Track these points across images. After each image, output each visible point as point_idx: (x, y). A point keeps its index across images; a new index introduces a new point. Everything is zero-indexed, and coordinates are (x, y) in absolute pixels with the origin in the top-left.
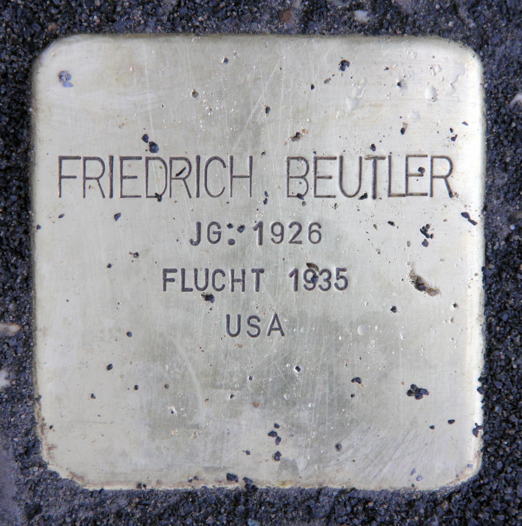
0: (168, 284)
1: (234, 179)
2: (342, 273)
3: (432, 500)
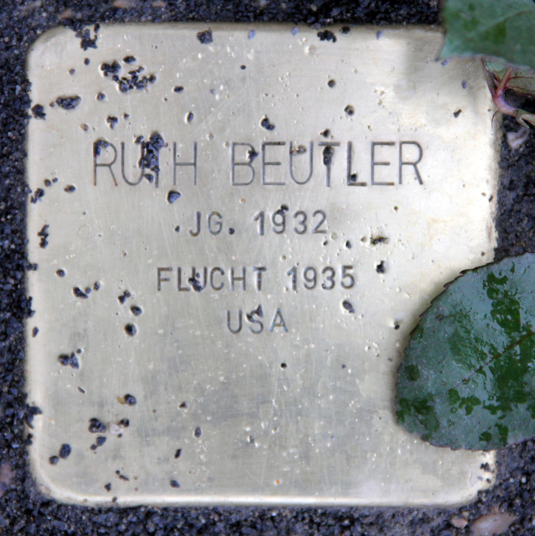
0: (162, 283)
1: (376, 167)
2: (350, 272)
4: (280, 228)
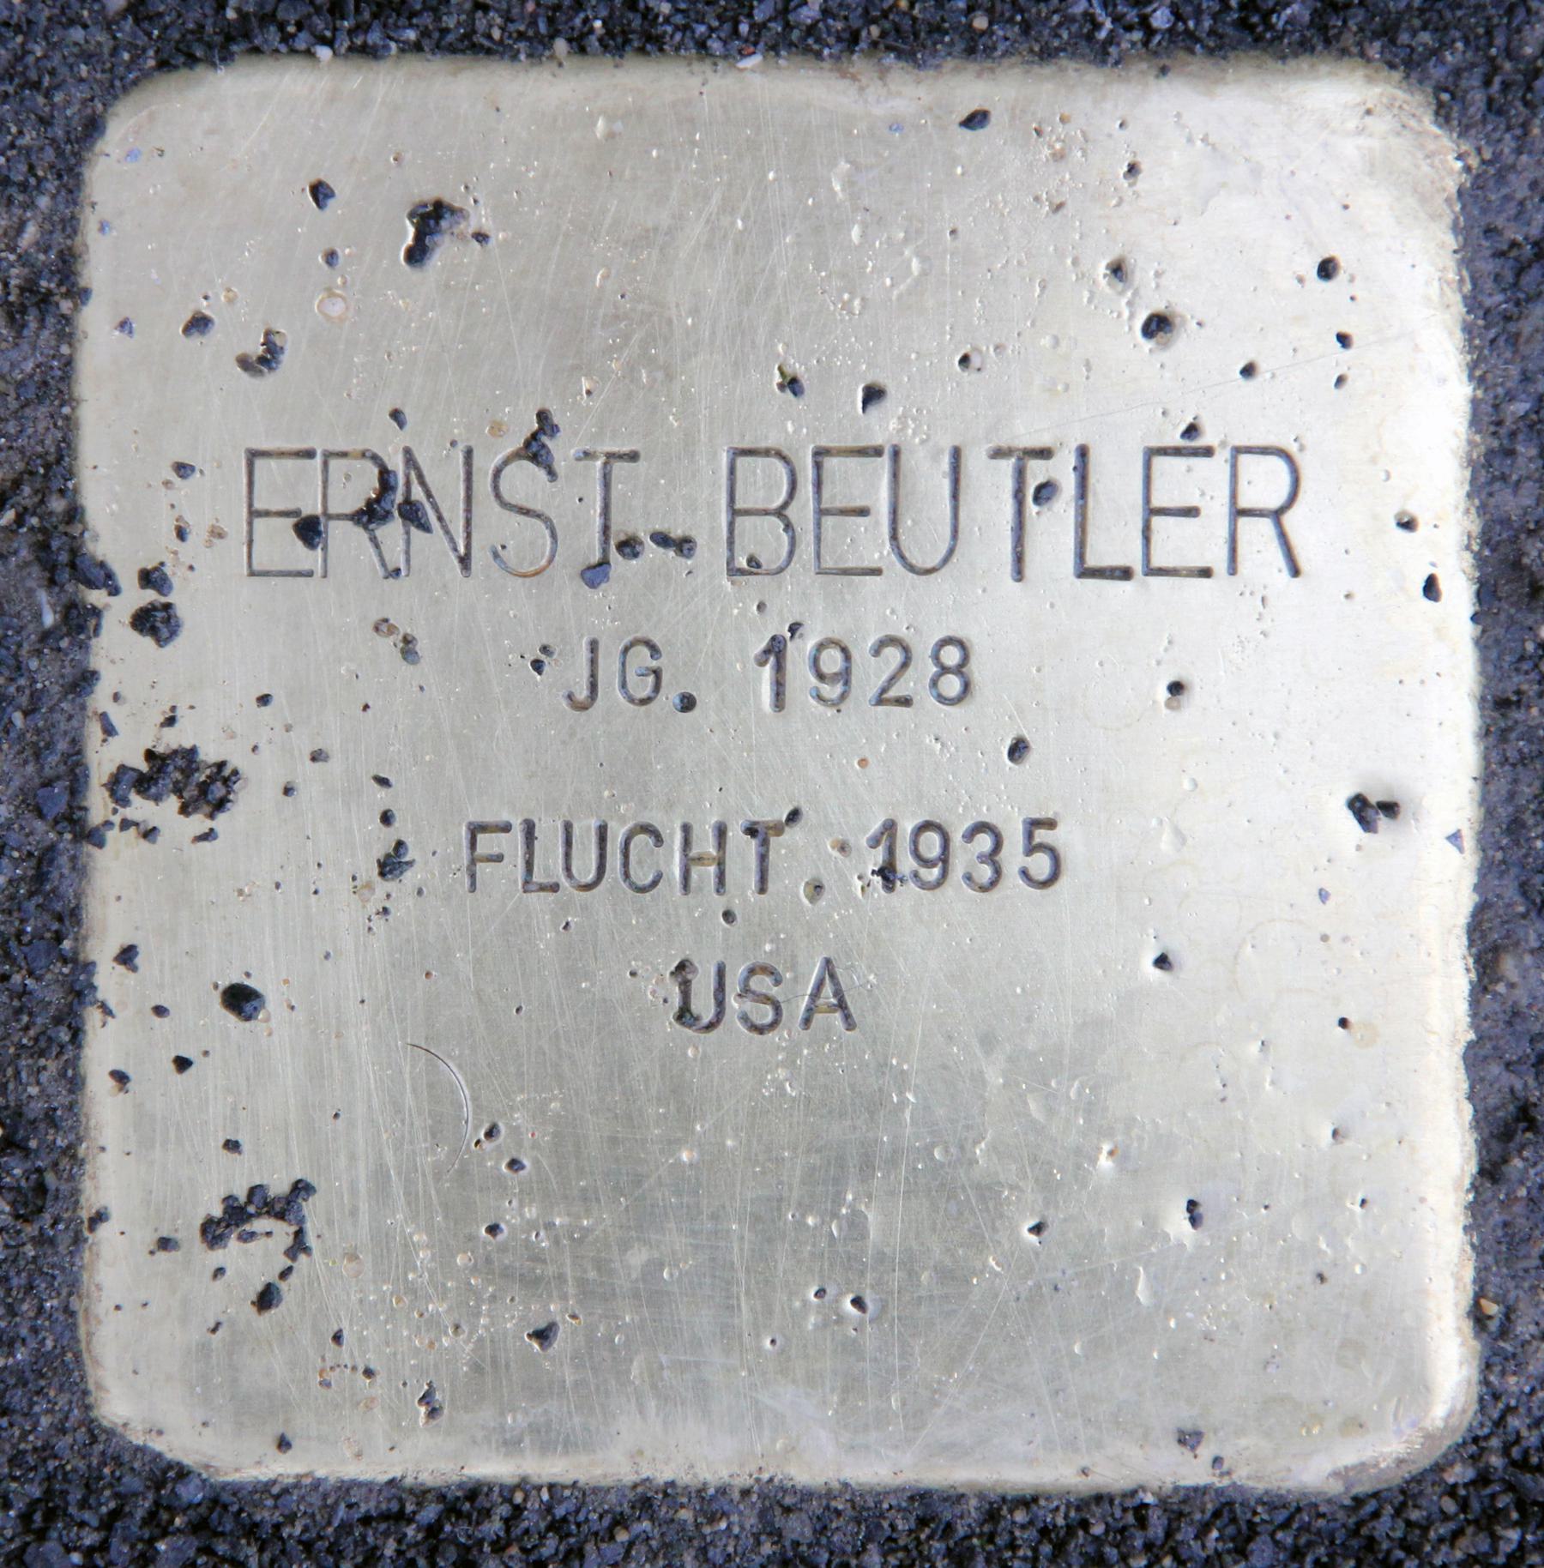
0: (483, 869)
2: (1041, 835)
3: (1293, 1515)
4: (832, 691)
